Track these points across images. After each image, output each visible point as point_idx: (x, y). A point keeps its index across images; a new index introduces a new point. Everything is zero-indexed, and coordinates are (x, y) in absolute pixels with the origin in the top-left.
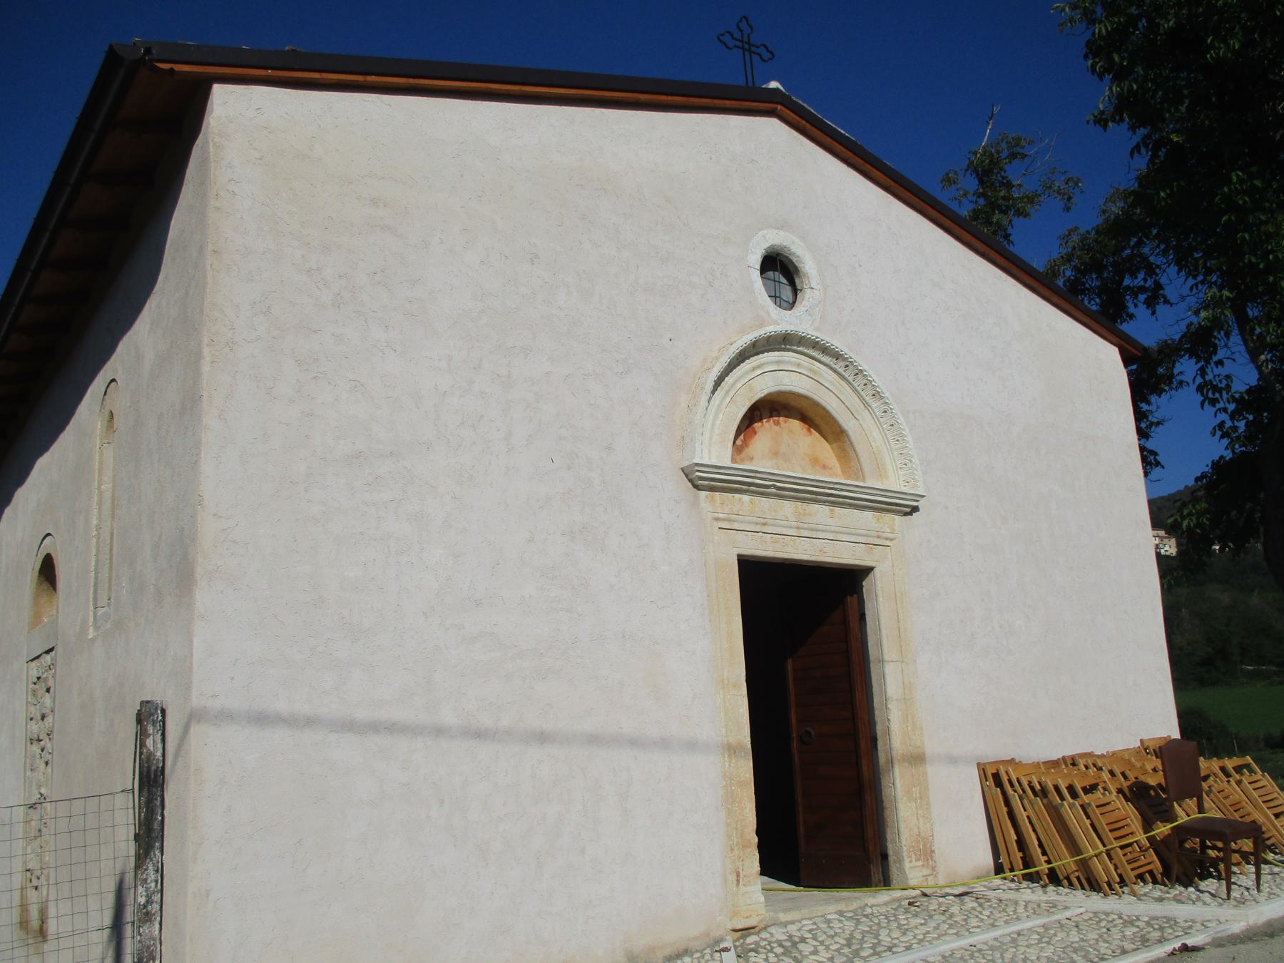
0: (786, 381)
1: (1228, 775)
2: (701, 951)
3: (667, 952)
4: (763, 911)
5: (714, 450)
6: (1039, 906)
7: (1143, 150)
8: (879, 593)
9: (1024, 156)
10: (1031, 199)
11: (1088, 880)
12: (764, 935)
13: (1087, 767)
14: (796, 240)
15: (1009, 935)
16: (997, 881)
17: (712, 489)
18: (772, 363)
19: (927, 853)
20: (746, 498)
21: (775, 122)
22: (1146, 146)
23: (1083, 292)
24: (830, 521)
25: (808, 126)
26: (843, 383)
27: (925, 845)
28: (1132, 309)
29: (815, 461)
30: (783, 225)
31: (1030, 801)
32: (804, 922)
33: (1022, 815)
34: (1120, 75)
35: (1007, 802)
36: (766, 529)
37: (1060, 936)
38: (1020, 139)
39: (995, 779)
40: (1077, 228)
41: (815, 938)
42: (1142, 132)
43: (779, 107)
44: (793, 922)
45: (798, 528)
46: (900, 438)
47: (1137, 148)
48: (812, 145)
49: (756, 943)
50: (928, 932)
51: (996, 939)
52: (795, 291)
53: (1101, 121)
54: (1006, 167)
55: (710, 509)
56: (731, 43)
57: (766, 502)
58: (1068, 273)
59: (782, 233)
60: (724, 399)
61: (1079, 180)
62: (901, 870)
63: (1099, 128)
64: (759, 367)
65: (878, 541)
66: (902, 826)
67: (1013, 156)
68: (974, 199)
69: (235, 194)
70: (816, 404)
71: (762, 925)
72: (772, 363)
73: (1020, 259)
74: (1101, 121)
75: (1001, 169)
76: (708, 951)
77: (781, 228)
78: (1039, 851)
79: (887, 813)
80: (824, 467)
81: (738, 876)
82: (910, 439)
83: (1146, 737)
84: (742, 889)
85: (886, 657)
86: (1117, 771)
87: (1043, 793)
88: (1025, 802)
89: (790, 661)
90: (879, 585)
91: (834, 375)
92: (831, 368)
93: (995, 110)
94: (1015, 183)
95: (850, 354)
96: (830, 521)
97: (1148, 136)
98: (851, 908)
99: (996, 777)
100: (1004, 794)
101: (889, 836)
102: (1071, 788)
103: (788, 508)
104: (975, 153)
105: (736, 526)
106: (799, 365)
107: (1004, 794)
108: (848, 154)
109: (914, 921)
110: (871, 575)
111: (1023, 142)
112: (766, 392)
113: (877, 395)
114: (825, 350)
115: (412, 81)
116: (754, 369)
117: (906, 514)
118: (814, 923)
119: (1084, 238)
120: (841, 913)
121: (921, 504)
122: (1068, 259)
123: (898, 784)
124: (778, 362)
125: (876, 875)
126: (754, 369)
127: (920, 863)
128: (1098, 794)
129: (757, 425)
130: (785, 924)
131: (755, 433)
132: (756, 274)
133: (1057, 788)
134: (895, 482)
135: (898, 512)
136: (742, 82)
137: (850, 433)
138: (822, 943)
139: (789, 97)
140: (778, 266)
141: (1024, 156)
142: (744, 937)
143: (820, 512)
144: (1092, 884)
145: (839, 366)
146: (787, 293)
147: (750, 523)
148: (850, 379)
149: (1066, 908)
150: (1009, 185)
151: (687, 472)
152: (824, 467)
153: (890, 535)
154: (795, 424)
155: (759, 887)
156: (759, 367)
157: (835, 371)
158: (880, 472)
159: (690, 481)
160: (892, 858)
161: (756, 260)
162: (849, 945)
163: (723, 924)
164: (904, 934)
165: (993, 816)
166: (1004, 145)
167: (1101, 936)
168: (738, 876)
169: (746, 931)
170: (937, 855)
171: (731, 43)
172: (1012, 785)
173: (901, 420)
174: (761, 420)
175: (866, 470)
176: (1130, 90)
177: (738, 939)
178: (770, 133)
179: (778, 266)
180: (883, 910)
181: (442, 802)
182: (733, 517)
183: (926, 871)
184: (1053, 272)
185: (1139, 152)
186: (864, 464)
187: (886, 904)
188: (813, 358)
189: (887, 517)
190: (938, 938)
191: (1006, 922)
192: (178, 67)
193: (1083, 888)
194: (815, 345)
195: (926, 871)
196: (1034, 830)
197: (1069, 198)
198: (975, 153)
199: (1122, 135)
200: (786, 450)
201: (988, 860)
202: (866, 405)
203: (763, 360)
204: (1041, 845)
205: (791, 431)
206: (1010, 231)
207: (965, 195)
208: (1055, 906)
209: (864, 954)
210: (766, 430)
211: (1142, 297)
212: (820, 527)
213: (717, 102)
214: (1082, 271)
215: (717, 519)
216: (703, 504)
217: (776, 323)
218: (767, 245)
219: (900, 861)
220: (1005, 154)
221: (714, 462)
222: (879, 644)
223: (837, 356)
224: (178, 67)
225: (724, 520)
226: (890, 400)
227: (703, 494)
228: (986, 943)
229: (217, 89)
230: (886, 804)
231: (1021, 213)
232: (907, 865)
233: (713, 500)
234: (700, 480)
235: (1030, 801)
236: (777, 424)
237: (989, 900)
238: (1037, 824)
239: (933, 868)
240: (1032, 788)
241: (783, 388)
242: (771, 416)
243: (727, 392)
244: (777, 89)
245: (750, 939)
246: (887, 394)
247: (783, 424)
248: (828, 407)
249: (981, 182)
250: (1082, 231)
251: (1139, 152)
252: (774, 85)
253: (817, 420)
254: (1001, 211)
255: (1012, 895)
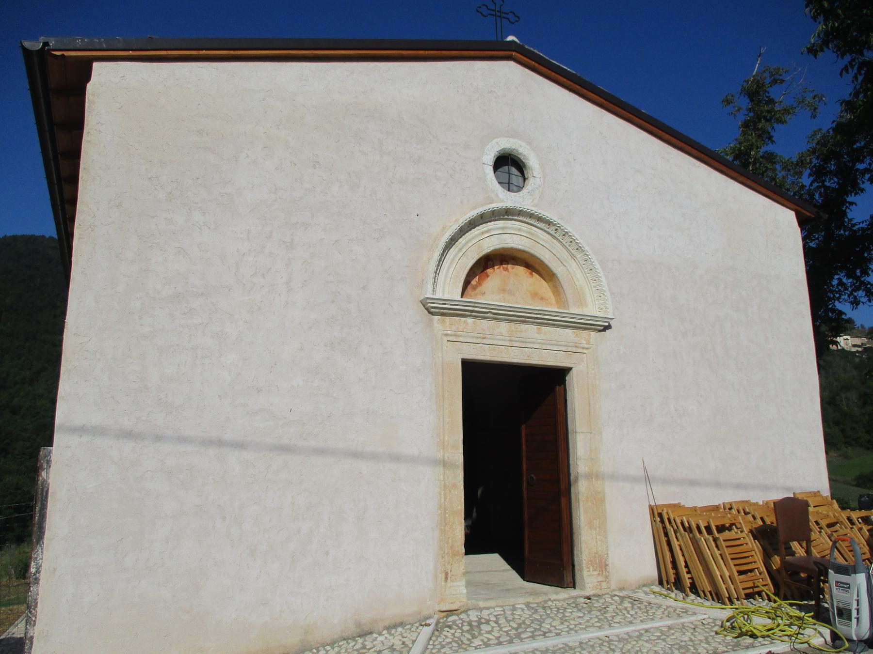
0: (509, 241)
1: (852, 523)
2: (412, 625)
3: (387, 623)
4: (465, 600)
5: (449, 289)
6: (675, 610)
7: (850, 70)
8: (575, 385)
9: (782, 81)
10: (786, 111)
11: (717, 594)
12: (463, 616)
13: (739, 511)
14: (523, 144)
15: (638, 631)
16: (657, 588)
17: (443, 314)
18: (498, 229)
19: (602, 566)
20: (470, 320)
21: (512, 63)
22: (852, 67)
23: (825, 174)
24: (537, 336)
25: (536, 65)
26: (555, 241)
27: (600, 561)
28: (862, 186)
29: (535, 295)
30: (514, 134)
31: (681, 535)
32: (497, 609)
33: (675, 543)
34: (828, 15)
35: (666, 534)
36: (485, 341)
37: (677, 635)
38: (779, 69)
39: (660, 518)
40: (820, 129)
41: (496, 622)
42: (847, 58)
43: (514, 54)
44: (487, 608)
45: (511, 341)
46: (596, 279)
47: (846, 69)
48: (541, 78)
49: (454, 622)
50: (580, 624)
51: (627, 633)
52: (525, 179)
53: (813, 51)
54: (769, 90)
55: (441, 328)
56: (510, 16)
57: (485, 323)
58: (814, 161)
59: (511, 140)
60: (457, 254)
61: (823, 96)
62: (582, 576)
63: (811, 56)
64: (487, 232)
65: (575, 350)
66: (583, 546)
67: (775, 82)
68: (746, 113)
69: (100, 131)
70: (533, 256)
71: (462, 609)
72: (498, 229)
73: (708, 149)
74: (813, 51)
75: (766, 91)
76: (417, 625)
77: (512, 136)
78: (685, 570)
79: (575, 537)
80: (542, 299)
81: (447, 574)
82: (603, 279)
83: (797, 491)
84: (449, 583)
85: (578, 430)
86: (758, 516)
87: (689, 530)
88: (678, 534)
89: (523, 427)
90: (575, 379)
91: (550, 237)
92: (546, 231)
93: (762, 50)
94: (777, 100)
95: (559, 221)
96: (537, 336)
97: (853, 60)
98: (537, 601)
99: (660, 515)
100: (664, 528)
101: (575, 552)
102: (708, 529)
103: (503, 327)
104: (747, 81)
105: (461, 339)
106: (519, 230)
107: (664, 528)
108: (569, 83)
109: (575, 615)
110: (571, 373)
111: (781, 72)
112: (492, 249)
113: (579, 249)
114: (540, 219)
115: (232, 52)
116: (483, 233)
117: (600, 331)
118: (504, 610)
119: (824, 136)
120: (527, 605)
121: (612, 323)
122: (813, 152)
123: (582, 518)
124: (503, 228)
125: (568, 579)
126: (483, 233)
127: (596, 573)
128: (732, 534)
129: (489, 271)
130: (481, 609)
131: (488, 276)
132: (490, 170)
133: (698, 527)
134: (592, 309)
135: (594, 330)
136: (494, 38)
137: (559, 276)
138: (499, 625)
139: (522, 47)
140: (509, 164)
141: (782, 81)
142: (447, 617)
143: (530, 330)
144: (717, 596)
145: (551, 230)
146: (516, 179)
147: (472, 337)
148: (560, 238)
149: (695, 614)
150: (771, 101)
151: (424, 303)
152: (542, 299)
153: (586, 346)
154: (520, 270)
155: (463, 583)
156: (487, 232)
157: (548, 233)
158: (581, 301)
159: (427, 309)
160: (577, 568)
161: (489, 158)
162: (516, 629)
163: (433, 606)
164: (562, 623)
165: (657, 542)
166: (767, 75)
167: (706, 638)
168: (447, 574)
169: (451, 612)
170: (610, 568)
171: (510, 16)
172: (670, 522)
173: (598, 266)
174: (493, 266)
175: (570, 301)
176: (833, 27)
177: (443, 618)
178: (509, 71)
179: (509, 164)
180: (559, 604)
181: (224, 518)
182: (459, 333)
183: (600, 579)
184: (802, 161)
185: (847, 72)
186: (568, 296)
187: (564, 600)
188: (531, 225)
189: (585, 334)
190: (584, 629)
191: (642, 621)
192: (67, 54)
193: (713, 600)
194: (531, 215)
195: (600, 579)
196: (683, 555)
197: (815, 109)
198: (747, 81)
199: (831, 60)
200: (504, 288)
201: (652, 572)
202: (573, 257)
203: (490, 227)
204: (687, 566)
205: (516, 274)
206: (772, 133)
207: (738, 110)
208: (686, 612)
209: (523, 636)
210: (496, 276)
211: (867, 176)
212: (528, 340)
213: (445, 52)
214: (826, 159)
215: (446, 335)
216: (436, 325)
217: (502, 201)
218: (500, 148)
219: (581, 570)
220: (768, 80)
221: (446, 297)
222: (574, 421)
223: (549, 223)
224: (67, 54)
225: (451, 335)
226: (589, 252)
227: (437, 318)
228: (617, 636)
229: (96, 65)
230: (575, 530)
231: (780, 121)
232: (585, 573)
233: (444, 322)
234: (434, 309)
235: (681, 535)
236: (507, 269)
237: (641, 603)
238: (685, 551)
239: (607, 577)
240: (682, 523)
241: (506, 246)
242: (501, 264)
243: (460, 249)
244: (513, 41)
245: (451, 619)
246: (587, 248)
247: (510, 270)
248: (542, 258)
249: (752, 100)
250: (824, 131)
251: (847, 72)
252: (510, 38)
253: (537, 266)
254: (767, 120)
255: (660, 600)
